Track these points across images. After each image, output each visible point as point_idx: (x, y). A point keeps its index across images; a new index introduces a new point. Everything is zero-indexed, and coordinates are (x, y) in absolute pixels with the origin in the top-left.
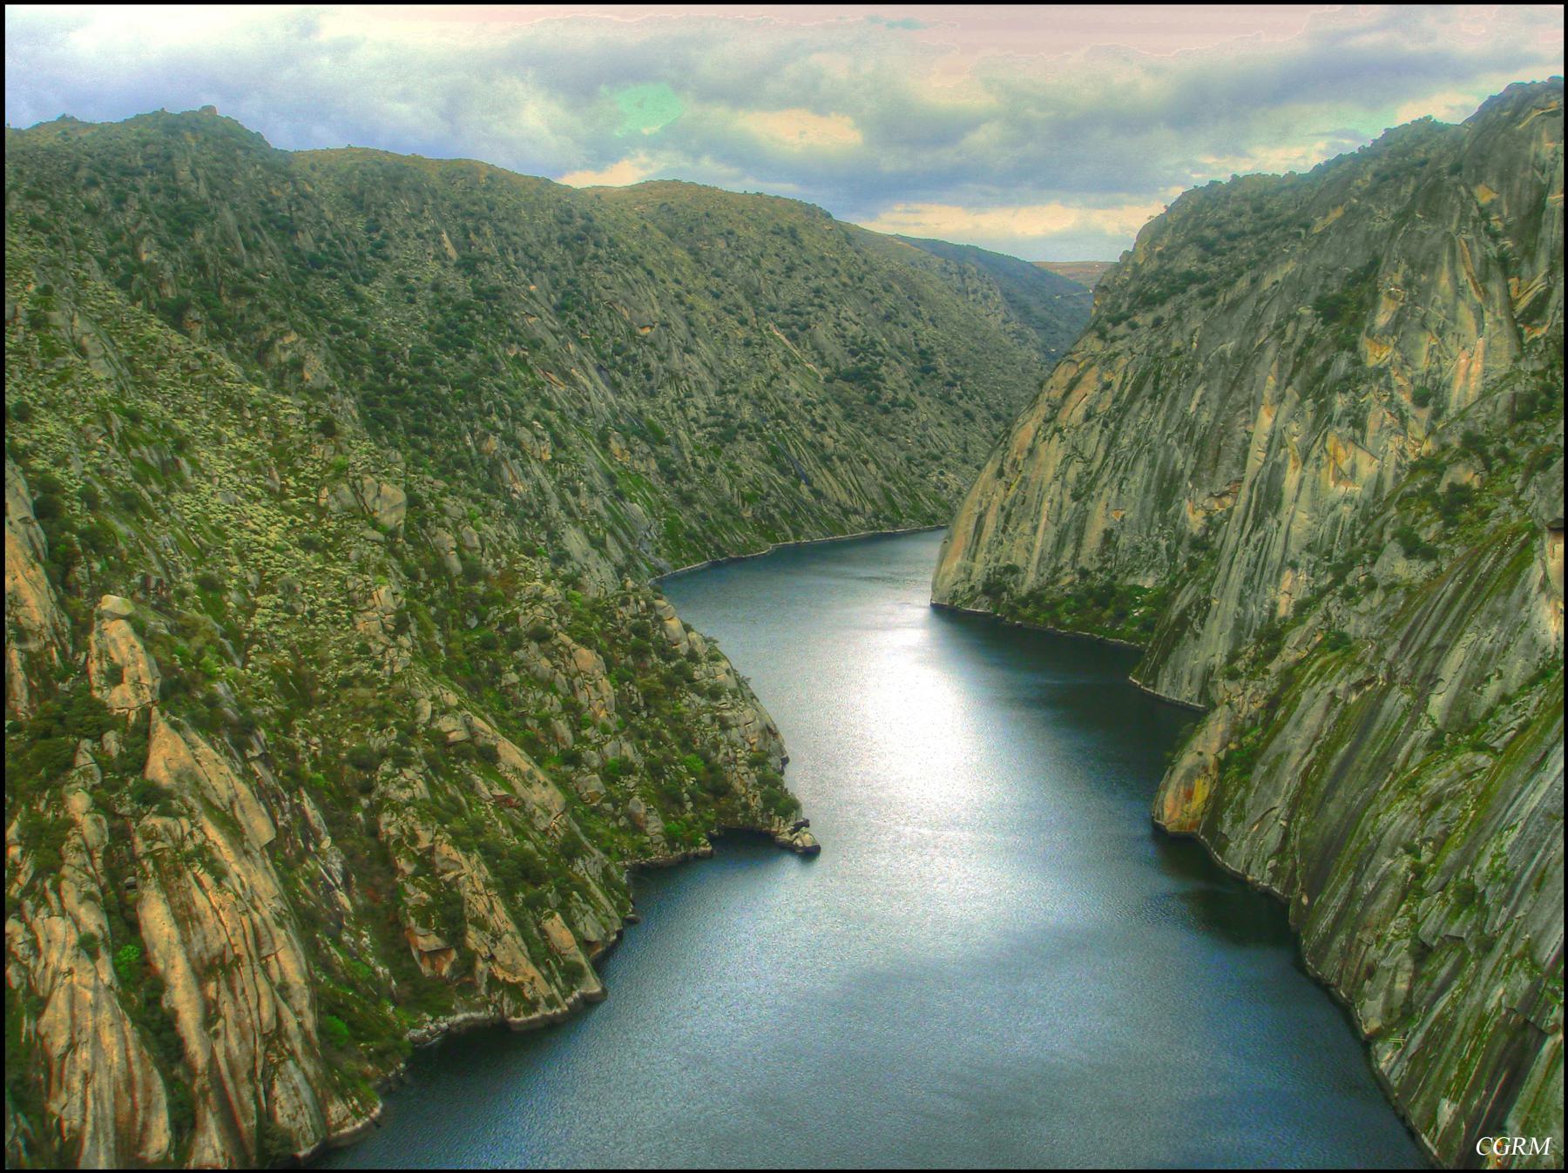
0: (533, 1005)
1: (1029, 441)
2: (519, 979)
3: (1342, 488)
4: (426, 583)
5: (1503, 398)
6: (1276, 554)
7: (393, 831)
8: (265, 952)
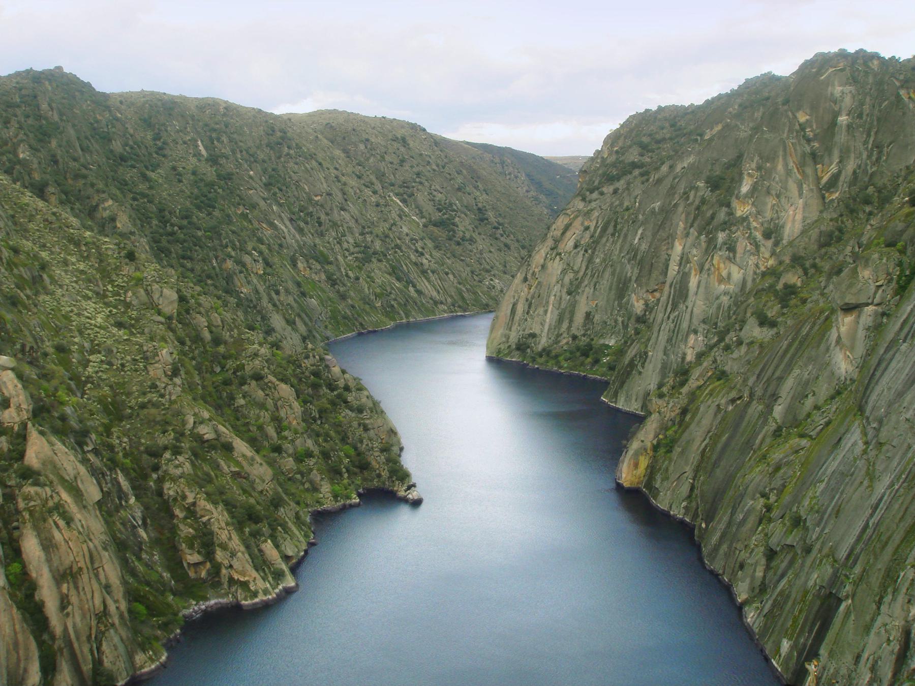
0: (255, 594)
2: (246, 579)
3: (723, 287)
4: (190, 347)
5: (814, 234)
6: (685, 325)
7: (171, 493)
8: (96, 565)
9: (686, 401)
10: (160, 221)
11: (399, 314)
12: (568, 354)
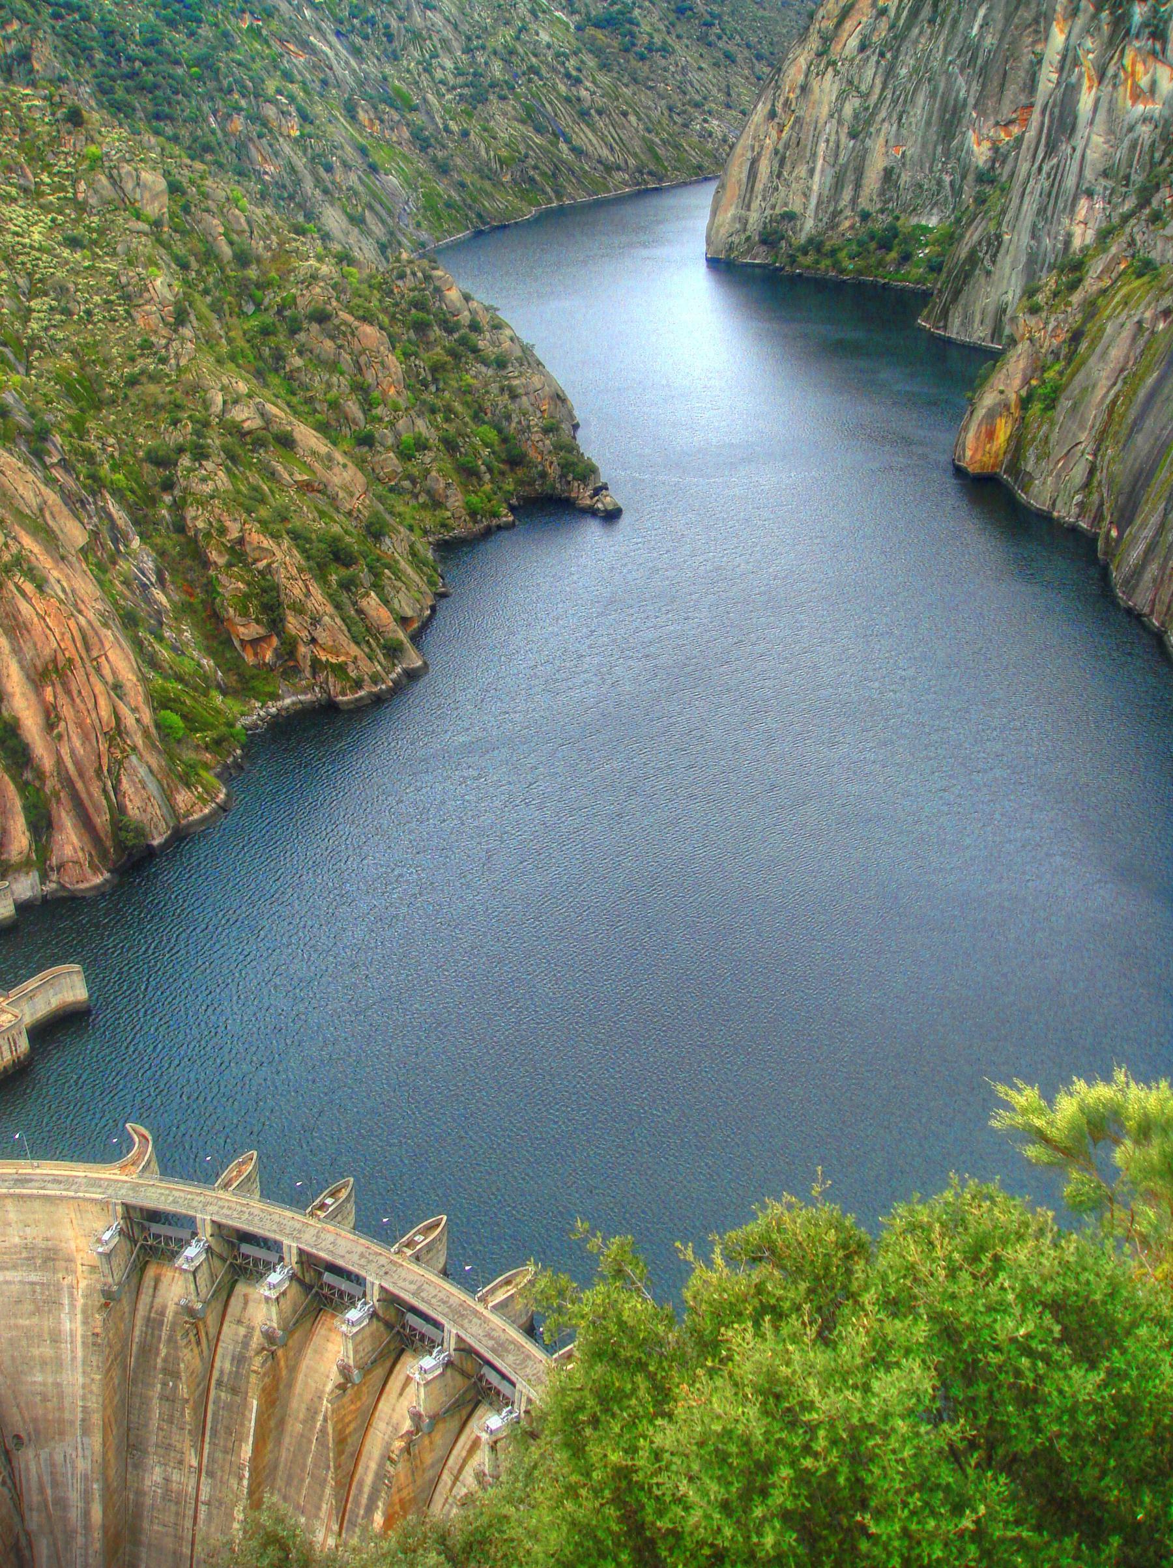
0: (358, 684)
1: (801, 79)
3: (1141, 107)
4: (198, 272)
6: (1070, 182)
7: (200, 524)
8: (95, 654)
9: (1079, 317)
10: (109, 54)
11: (544, 192)
12: (855, 247)
